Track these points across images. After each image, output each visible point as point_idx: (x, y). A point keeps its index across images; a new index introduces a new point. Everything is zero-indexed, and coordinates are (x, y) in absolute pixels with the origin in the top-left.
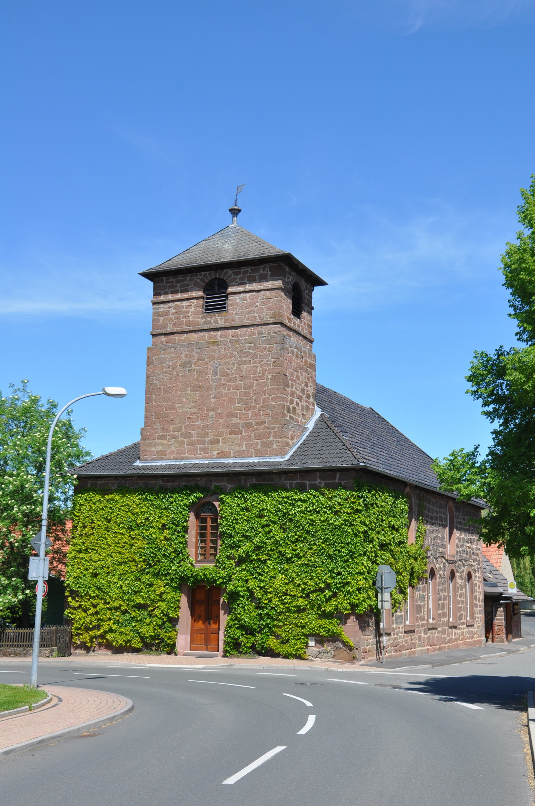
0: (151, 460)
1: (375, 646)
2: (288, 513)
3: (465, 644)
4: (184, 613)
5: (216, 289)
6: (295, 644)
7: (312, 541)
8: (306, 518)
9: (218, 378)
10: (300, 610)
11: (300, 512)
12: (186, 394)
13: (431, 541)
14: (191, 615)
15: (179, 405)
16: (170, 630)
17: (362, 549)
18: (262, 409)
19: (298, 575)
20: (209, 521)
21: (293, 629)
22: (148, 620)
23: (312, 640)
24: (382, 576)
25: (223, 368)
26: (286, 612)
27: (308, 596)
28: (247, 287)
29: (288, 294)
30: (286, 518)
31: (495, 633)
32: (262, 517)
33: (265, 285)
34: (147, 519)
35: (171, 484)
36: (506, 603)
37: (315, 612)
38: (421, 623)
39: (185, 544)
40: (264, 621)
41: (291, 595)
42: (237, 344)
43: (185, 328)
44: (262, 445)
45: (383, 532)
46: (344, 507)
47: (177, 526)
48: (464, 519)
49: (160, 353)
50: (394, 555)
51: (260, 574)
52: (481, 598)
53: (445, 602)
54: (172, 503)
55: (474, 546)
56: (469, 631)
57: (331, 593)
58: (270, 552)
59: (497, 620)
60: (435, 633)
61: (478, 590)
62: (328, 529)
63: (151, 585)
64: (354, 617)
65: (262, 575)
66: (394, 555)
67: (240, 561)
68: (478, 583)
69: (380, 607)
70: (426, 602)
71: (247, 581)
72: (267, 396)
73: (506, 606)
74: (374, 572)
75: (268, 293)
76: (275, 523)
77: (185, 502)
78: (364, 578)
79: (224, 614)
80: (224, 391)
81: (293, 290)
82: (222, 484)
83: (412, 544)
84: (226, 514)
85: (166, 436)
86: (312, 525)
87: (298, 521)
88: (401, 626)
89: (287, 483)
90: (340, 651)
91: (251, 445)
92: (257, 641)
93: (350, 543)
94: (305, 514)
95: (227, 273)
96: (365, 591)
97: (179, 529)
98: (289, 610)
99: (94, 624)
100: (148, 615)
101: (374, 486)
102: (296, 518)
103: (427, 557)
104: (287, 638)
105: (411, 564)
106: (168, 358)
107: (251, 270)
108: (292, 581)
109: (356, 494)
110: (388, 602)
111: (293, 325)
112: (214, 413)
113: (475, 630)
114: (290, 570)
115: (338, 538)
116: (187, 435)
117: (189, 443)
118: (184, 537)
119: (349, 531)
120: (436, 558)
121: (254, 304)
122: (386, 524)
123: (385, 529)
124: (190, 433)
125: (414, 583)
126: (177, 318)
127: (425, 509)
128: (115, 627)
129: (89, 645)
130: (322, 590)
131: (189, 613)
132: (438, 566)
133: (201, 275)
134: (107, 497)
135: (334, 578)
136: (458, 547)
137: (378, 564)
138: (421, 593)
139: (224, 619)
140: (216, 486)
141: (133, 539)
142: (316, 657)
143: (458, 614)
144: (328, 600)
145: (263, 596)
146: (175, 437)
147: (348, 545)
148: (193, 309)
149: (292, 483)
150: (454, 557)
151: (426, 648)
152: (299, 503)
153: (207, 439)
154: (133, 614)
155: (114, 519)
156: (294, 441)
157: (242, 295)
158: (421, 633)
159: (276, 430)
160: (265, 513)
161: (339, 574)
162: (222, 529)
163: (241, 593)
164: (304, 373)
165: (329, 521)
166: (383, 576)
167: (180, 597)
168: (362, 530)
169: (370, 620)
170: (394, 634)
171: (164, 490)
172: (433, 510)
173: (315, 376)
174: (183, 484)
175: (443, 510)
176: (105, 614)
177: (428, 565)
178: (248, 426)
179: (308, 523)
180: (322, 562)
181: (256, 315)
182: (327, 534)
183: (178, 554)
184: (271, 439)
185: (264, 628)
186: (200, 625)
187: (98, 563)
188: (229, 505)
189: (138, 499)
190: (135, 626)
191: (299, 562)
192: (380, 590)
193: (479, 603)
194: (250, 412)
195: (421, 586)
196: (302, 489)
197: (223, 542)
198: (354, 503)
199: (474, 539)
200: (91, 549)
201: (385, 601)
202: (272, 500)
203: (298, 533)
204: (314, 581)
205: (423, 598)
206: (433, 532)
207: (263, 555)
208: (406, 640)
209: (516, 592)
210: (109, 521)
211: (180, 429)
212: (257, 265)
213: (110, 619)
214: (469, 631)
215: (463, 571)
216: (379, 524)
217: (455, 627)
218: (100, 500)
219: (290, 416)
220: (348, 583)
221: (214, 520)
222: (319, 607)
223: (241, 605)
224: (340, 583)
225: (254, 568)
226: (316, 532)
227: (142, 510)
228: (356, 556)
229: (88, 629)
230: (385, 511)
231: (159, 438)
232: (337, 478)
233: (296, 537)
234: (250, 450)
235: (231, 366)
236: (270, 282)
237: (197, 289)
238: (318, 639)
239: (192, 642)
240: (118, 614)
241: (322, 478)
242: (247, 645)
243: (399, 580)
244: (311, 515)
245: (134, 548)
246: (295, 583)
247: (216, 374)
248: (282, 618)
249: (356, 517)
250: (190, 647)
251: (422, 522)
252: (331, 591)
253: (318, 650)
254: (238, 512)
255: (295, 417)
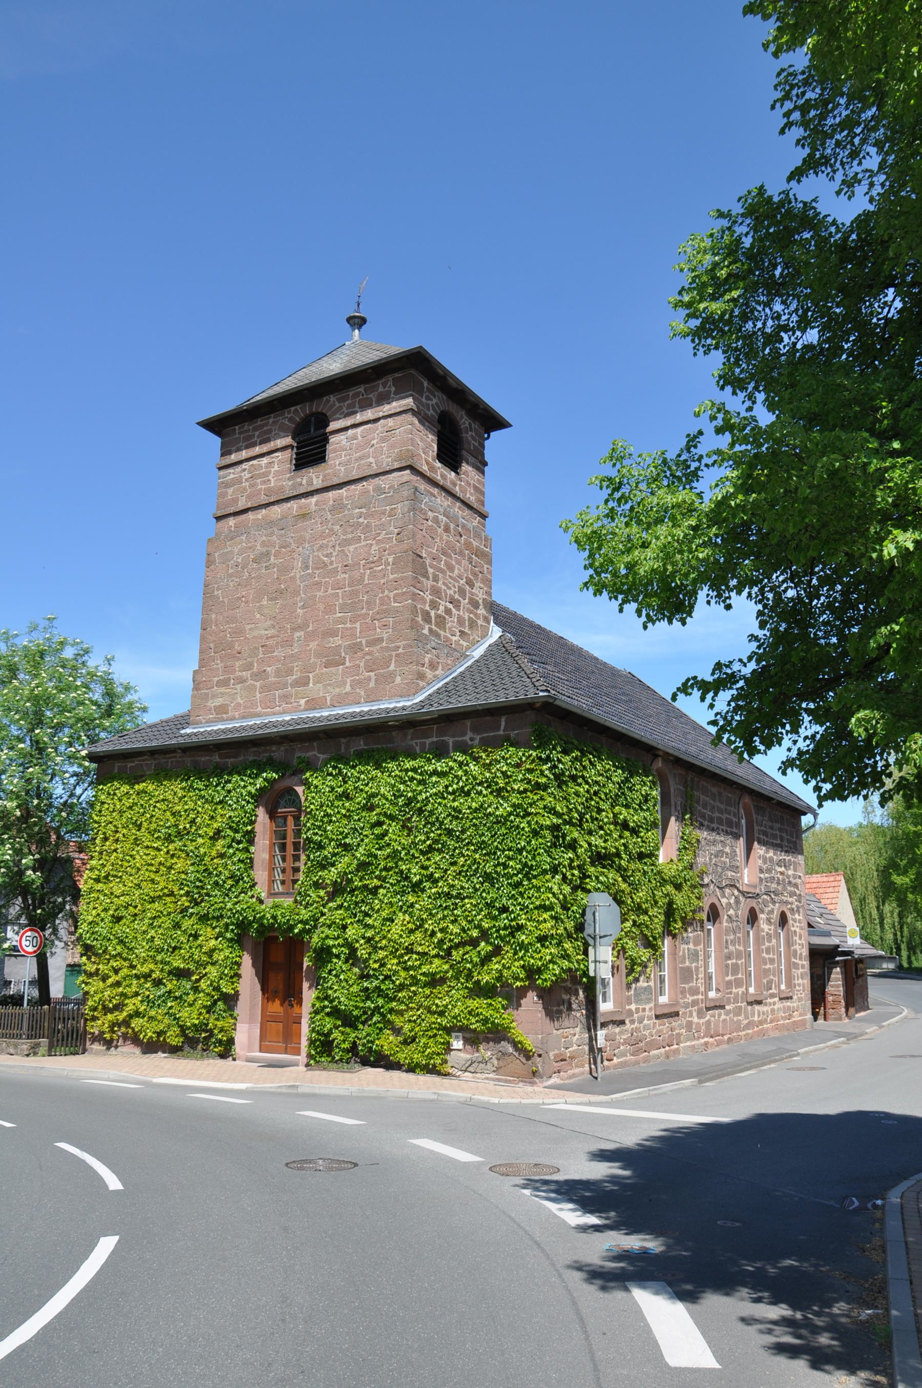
0: (207, 722)
1: (587, 1048)
2: (415, 798)
3: (777, 1028)
4: (248, 984)
5: (312, 430)
6: (426, 1046)
7: (456, 848)
8: (445, 806)
9: (309, 574)
10: (435, 981)
11: (436, 794)
12: (261, 607)
13: (710, 859)
14: (263, 989)
15: (249, 627)
16: (224, 1015)
17: (549, 860)
18: (378, 617)
19: (431, 914)
20: (290, 820)
21: (423, 1017)
22: (191, 998)
23: (457, 1037)
24: (594, 914)
25: (318, 556)
26: (411, 985)
27: (449, 953)
28: (359, 418)
29: (427, 424)
30: (412, 808)
31: (829, 1006)
32: (371, 808)
33: (387, 409)
34: (193, 822)
35: (232, 760)
36: (845, 961)
37: (462, 984)
38: (691, 998)
39: (250, 864)
40: (372, 1002)
41: (418, 953)
42: (340, 513)
43: (264, 499)
44: (376, 680)
45: (602, 832)
46: (515, 780)
47: (236, 831)
48: (771, 828)
49: (226, 545)
50: (629, 877)
51: (366, 915)
52: (804, 954)
53: (739, 962)
54: (229, 792)
55: (791, 872)
56: (784, 1007)
57: (490, 948)
58: (384, 873)
59: (832, 986)
60: (720, 1015)
61: (798, 941)
62: (485, 825)
63: (196, 936)
64: (535, 993)
65: (370, 916)
66: (629, 877)
67: (337, 890)
68: (798, 930)
69: (592, 974)
70: (701, 963)
71: (344, 927)
72: (386, 592)
73: (845, 965)
74: (579, 907)
75: (390, 422)
76: (392, 818)
77: (249, 788)
78: (552, 917)
79: (310, 988)
80: (318, 594)
81: (439, 421)
82: (310, 754)
83: (672, 860)
84: (312, 807)
85: (229, 679)
86: (457, 818)
87: (431, 813)
88: (647, 1007)
89: (416, 744)
90: (509, 1059)
91: (359, 682)
92: (359, 1039)
93: (524, 848)
94: (445, 799)
95: (328, 401)
96: (554, 942)
97: (238, 836)
98: (415, 982)
99: (114, 1002)
100: (191, 989)
101: (576, 742)
102: (429, 807)
103: (702, 886)
104: (413, 1033)
105: (668, 895)
106: (236, 551)
107: (365, 390)
108: (421, 926)
109: (534, 754)
110: (606, 962)
111: (439, 478)
112: (302, 633)
113: (795, 1005)
114: (417, 906)
115: (503, 840)
116: (261, 675)
117: (264, 689)
118: (247, 850)
119: (522, 825)
120: (720, 888)
121: (368, 444)
122: (607, 817)
123: (606, 828)
124: (265, 671)
125: (675, 928)
126: (252, 486)
127: (698, 802)
128: (143, 1008)
129: (107, 1036)
130: (474, 943)
131: (258, 987)
132: (724, 901)
133: (289, 412)
134: (136, 787)
135: (495, 918)
136: (761, 871)
137: (589, 891)
138: (691, 946)
139: (309, 995)
140: (300, 757)
141: (173, 856)
142: (465, 1071)
143: (765, 981)
144: (486, 960)
145: (370, 954)
146: (242, 681)
147: (521, 854)
148: (276, 468)
149: (425, 743)
150: (755, 887)
151: (702, 1041)
152: (434, 779)
153: (290, 679)
154: (169, 986)
155: (145, 825)
156: (437, 673)
157: (350, 432)
158: (691, 1016)
159: (401, 650)
160: (376, 800)
161: (504, 909)
162: (306, 833)
163: (334, 950)
164: (465, 562)
165: (486, 809)
166: (597, 914)
167: (240, 956)
168: (548, 823)
169: (573, 998)
170: (632, 1022)
171: (220, 771)
172: (713, 807)
173: (490, 572)
174: (251, 758)
175: (732, 809)
176: (130, 986)
177: (706, 899)
178: (355, 648)
179: (450, 815)
180: (474, 888)
181: (371, 460)
182: (483, 834)
183: (237, 882)
184: (392, 667)
185: (373, 1015)
186: (276, 1007)
187: (122, 898)
188: (317, 790)
189: (181, 789)
190: (171, 1008)
191: (433, 890)
192: (591, 941)
193: (800, 962)
194: (358, 625)
195: (690, 935)
196: (441, 752)
197: (308, 856)
198: (530, 771)
199: (790, 860)
200: (113, 876)
201: (603, 960)
202: (389, 776)
203: (432, 835)
204: (460, 924)
205: (695, 956)
206: (714, 842)
207: (372, 879)
208: (658, 1031)
209: (858, 943)
210: (139, 827)
211: (249, 667)
212: (374, 380)
213: (137, 994)
214: (784, 1007)
215: (772, 912)
216: (591, 817)
217: (759, 1003)
218: (127, 793)
219: (430, 630)
220: (520, 928)
221: (297, 818)
222: (469, 976)
223: (334, 972)
224: (505, 928)
225: (356, 903)
226: (463, 831)
227: (186, 807)
228: (535, 873)
229: (106, 1010)
230: (606, 794)
231: (220, 684)
232: (502, 728)
233: (428, 843)
234: (358, 690)
235: (330, 550)
236: (394, 404)
237: (282, 434)
238: (468, 1035)
239: (263, 1037)
240: (147, 986)
241: (475, 730)
242: (343, 1046)
243: (641, 924)
244: (454, 800)
245: (173, 872)
246: (426, 930)
247: (307, 567)
248: (404, 997)
249: (536, 798)
250: (261, 1045)
251: (692, 825)
252: (491, 944)
253: (468, 1056)
254: (332, 802)
255: (442, 633)
